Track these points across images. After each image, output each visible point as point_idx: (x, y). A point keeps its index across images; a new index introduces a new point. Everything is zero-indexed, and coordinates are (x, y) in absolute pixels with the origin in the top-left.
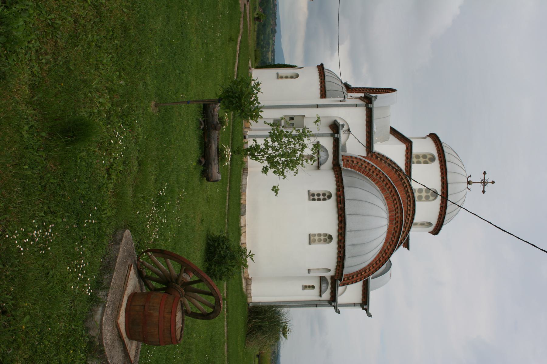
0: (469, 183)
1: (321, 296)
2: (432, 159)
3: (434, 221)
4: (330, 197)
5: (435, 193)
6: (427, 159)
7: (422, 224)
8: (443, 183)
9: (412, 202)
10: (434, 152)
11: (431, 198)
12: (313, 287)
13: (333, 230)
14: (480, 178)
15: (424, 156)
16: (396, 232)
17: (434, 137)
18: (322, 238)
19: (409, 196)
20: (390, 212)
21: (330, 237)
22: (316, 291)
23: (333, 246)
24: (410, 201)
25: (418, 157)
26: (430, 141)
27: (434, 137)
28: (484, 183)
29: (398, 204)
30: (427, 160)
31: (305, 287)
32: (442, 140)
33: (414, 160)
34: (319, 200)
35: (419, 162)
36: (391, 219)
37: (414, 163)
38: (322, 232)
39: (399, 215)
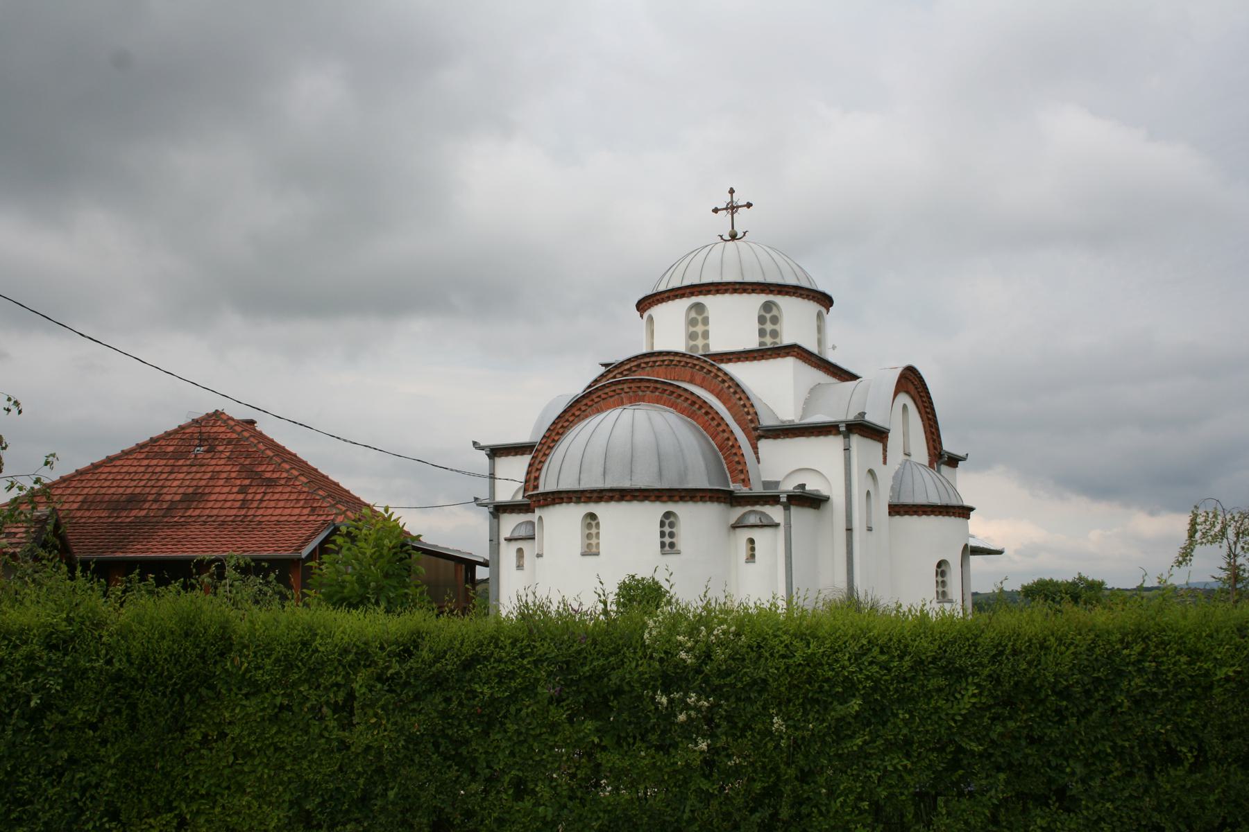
0: (734, 237)
1: (777, 525)
2: (699, 307)
3: (812, 307)
4: (592, 516)
5: (767, 306)
6: (698, 316)
7: (820, 330)
8: (676, 297)
9: (647, 360)
10: (683, 304)
11: (775, 312)
12: (752, 541)
13: (655, 511)
14: (724, 216)
15: (692, 322)
16: (657, 388)
17: (644, 304)
18: (667, 529)
19: (638, 366)
20: (622, 403)
21: (668, 515)
22: (760, 536)
23: (603, 511)
24: (647, 363)
25: (692, 336)
26: (658, 311)
27: (644, 304)
28: (732, 208)
29: (607, 390)
30: (700, 318)
31: (752, 557)
32: (649, 292)
33: (769, 342)
34: (662, 534)
35: (706, 335)
36: (635, 399)
37: (706, 346)
38: (657, 529)
39: (625, 386)
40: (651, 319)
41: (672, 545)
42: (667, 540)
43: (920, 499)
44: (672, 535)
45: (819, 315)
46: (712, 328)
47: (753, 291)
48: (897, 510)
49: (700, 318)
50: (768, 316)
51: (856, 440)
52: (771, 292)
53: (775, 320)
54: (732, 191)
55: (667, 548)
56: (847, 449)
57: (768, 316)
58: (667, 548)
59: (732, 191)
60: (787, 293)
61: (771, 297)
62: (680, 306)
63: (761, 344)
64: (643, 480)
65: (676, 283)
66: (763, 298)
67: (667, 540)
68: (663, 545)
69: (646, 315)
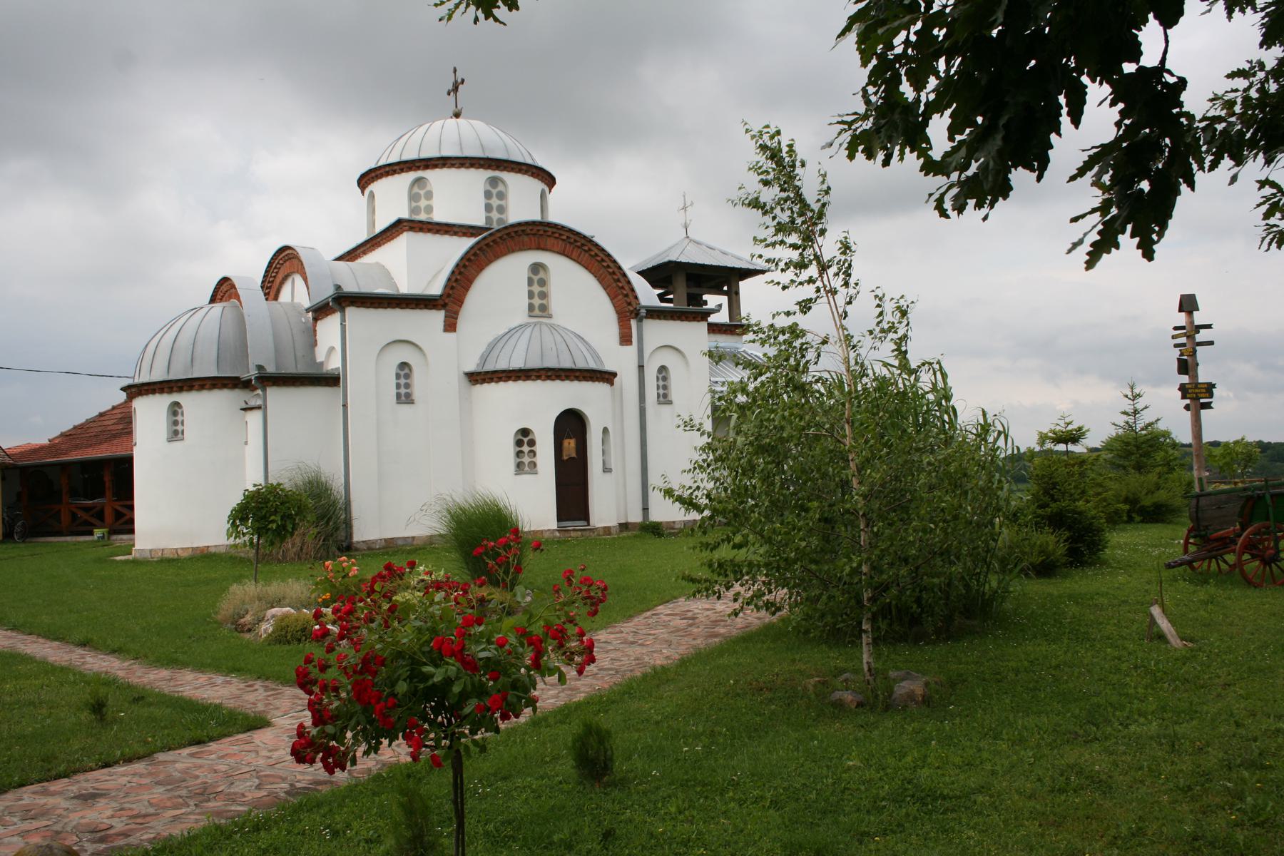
3: (537, 185)
17: (366, 180)
26: (377, 187)
30: (422, 192)
32: (373, 166)
40: (372, 195)
41: (408, 396)
42: (403, 391)
43: (502, 365)
44: (407, 386)
45: (543, 196)
46: (435, 203)
47: (402, 171)
48: (477, 378)
49: (422, 192)
50: (418, 192)
51: (351, 312)
52: (418, 168)
53: (501, 196)
54: (455, 71)
55: (537, 312)
56: (645, 509)
57: (494, 192)
58: (537, 312)
59: (455, 71)
60: (435, 166)
61: (420, 174)
62: (404, 180)
63: (488, 219)
64: (158, 375)
65: (394, 158)
66: (411, 176)
67: (403, 391)
68: (398, 396)
69: (367, 191)
